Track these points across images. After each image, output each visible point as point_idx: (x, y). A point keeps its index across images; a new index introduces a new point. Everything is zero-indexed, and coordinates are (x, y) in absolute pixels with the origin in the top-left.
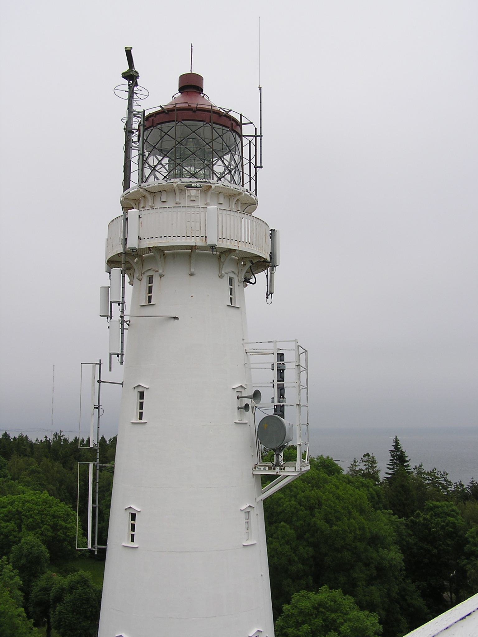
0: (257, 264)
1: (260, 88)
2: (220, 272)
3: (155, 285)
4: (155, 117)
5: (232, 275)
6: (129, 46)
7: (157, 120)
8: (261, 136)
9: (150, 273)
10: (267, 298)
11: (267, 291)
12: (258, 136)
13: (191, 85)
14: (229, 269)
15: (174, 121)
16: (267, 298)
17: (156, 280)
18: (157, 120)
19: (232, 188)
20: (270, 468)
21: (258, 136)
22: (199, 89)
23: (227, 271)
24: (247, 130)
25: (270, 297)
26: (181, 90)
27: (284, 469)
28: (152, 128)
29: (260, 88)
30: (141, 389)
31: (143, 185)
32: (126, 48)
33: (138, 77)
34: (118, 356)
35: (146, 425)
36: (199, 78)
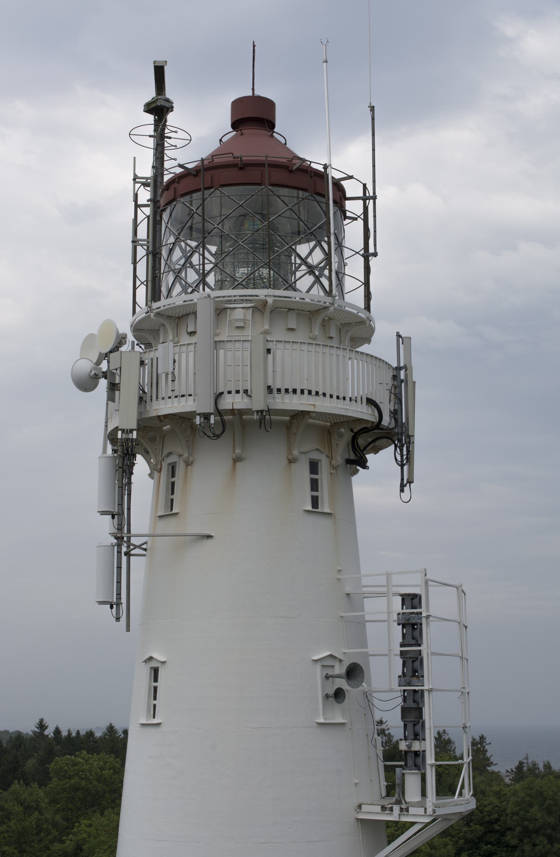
0: (376, 432)
1: (372, 109)
2: (290, 452)
3: (178, 479)
4: (178, 183)
5: (315, 456)
6: (160, 58)
7: (182, 187)
8: (374, 198)
9: (171, 460)
10: (402, 490)
11: (402, 479)
12: (369, 198)
13: (254, 116)
14: (308, 447)
15: (199, 190)
16: (402, 490)
17: (180, 469)
18: (182, 187)
19: (298, 299)
20: (383, 808)
21: (369, 198)
22: (268, 124)
23: (304, 449)
24: (352, 189)
25: (406, 489)
26: (235, 125)
27: (407, 810)
28: (174, 203)
29: (372, 109)
30: (154, 664)
31: (155, 305)
32: (154, 62)
33: (170, 109)
34: (112, 607)
35: (162, 729)
36: (269, 105)
